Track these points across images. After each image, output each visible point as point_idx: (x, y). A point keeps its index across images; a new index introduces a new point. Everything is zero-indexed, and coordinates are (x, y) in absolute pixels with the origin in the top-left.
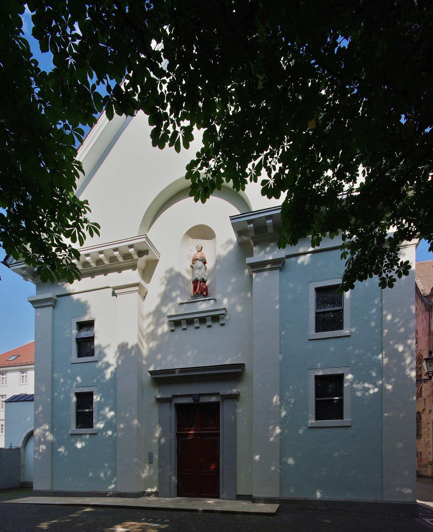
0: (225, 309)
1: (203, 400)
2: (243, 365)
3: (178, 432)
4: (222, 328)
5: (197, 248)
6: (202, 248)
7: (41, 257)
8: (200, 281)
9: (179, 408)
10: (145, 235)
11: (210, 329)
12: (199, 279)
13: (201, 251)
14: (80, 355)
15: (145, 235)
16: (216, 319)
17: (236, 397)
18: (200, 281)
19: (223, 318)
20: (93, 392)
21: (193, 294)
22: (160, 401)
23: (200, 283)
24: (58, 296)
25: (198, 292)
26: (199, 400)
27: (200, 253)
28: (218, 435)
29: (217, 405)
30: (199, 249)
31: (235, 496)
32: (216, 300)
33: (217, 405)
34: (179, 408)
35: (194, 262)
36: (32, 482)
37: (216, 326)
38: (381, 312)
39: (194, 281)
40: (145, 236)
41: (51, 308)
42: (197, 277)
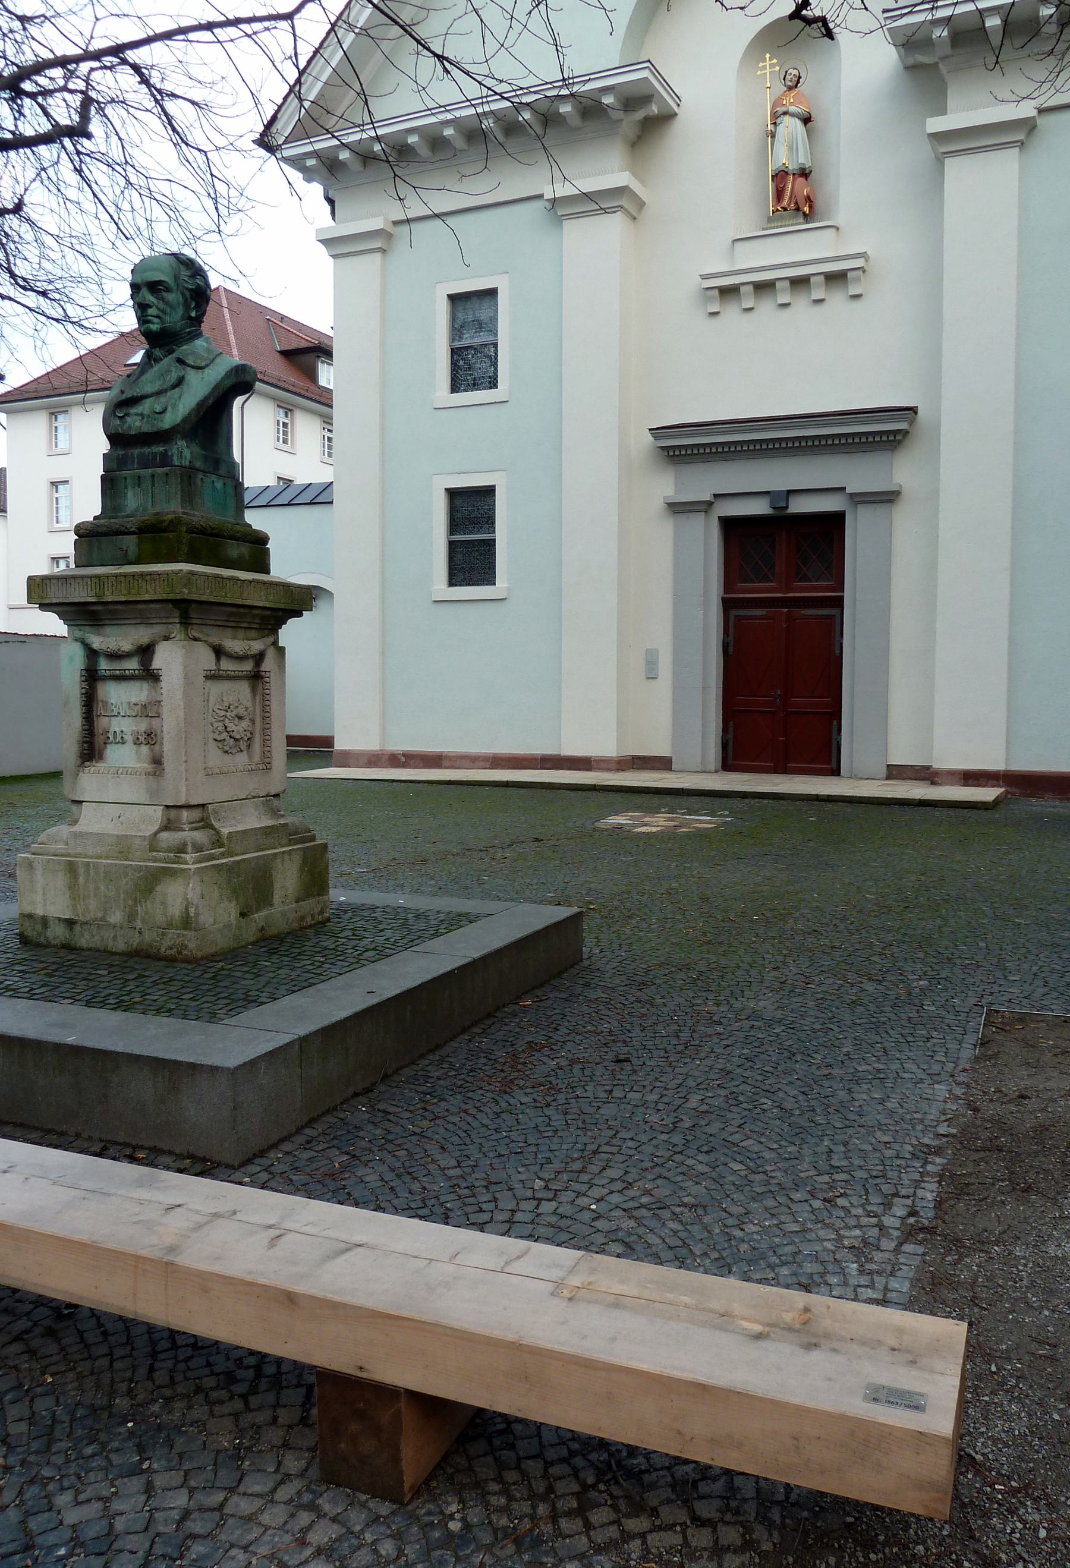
0: (863, 255)
1: (800, 506)
2: (913, 410)
3: (726, 596)
4: (856, 305)
5: (784, 79)
6: (800, 77)
7: (69, 67)
8: (794, 174)
9: (729, 524)
10: (649, 61)
11: (819, 308)
12: (790, 168)
13: (796, 86)
14: (455, 388)
15: (649, 61)
16: (837, 279)
17: (888, 498)
18: (794, 174)
19: (858, 280)
20: (494, 486)
21: (773, 212)
22: (677, 508)
23: (794, 180)
24: (1041, 111)
25: (789, 205)
26: (787, 507)
27: (793, 93)
28: (839, 602)
29: (834, 522)
30: (790, 84)
31: (884, 771)
32: (838, 229)
33: (834, 522)
34: (729, 524)
35: (778, 121)
36: (332, 738)
37: (837, 300)
38: (158, 87)
39: (777, 174)
40: (648, 64)
41: (378, 256)
42: (784, 164)
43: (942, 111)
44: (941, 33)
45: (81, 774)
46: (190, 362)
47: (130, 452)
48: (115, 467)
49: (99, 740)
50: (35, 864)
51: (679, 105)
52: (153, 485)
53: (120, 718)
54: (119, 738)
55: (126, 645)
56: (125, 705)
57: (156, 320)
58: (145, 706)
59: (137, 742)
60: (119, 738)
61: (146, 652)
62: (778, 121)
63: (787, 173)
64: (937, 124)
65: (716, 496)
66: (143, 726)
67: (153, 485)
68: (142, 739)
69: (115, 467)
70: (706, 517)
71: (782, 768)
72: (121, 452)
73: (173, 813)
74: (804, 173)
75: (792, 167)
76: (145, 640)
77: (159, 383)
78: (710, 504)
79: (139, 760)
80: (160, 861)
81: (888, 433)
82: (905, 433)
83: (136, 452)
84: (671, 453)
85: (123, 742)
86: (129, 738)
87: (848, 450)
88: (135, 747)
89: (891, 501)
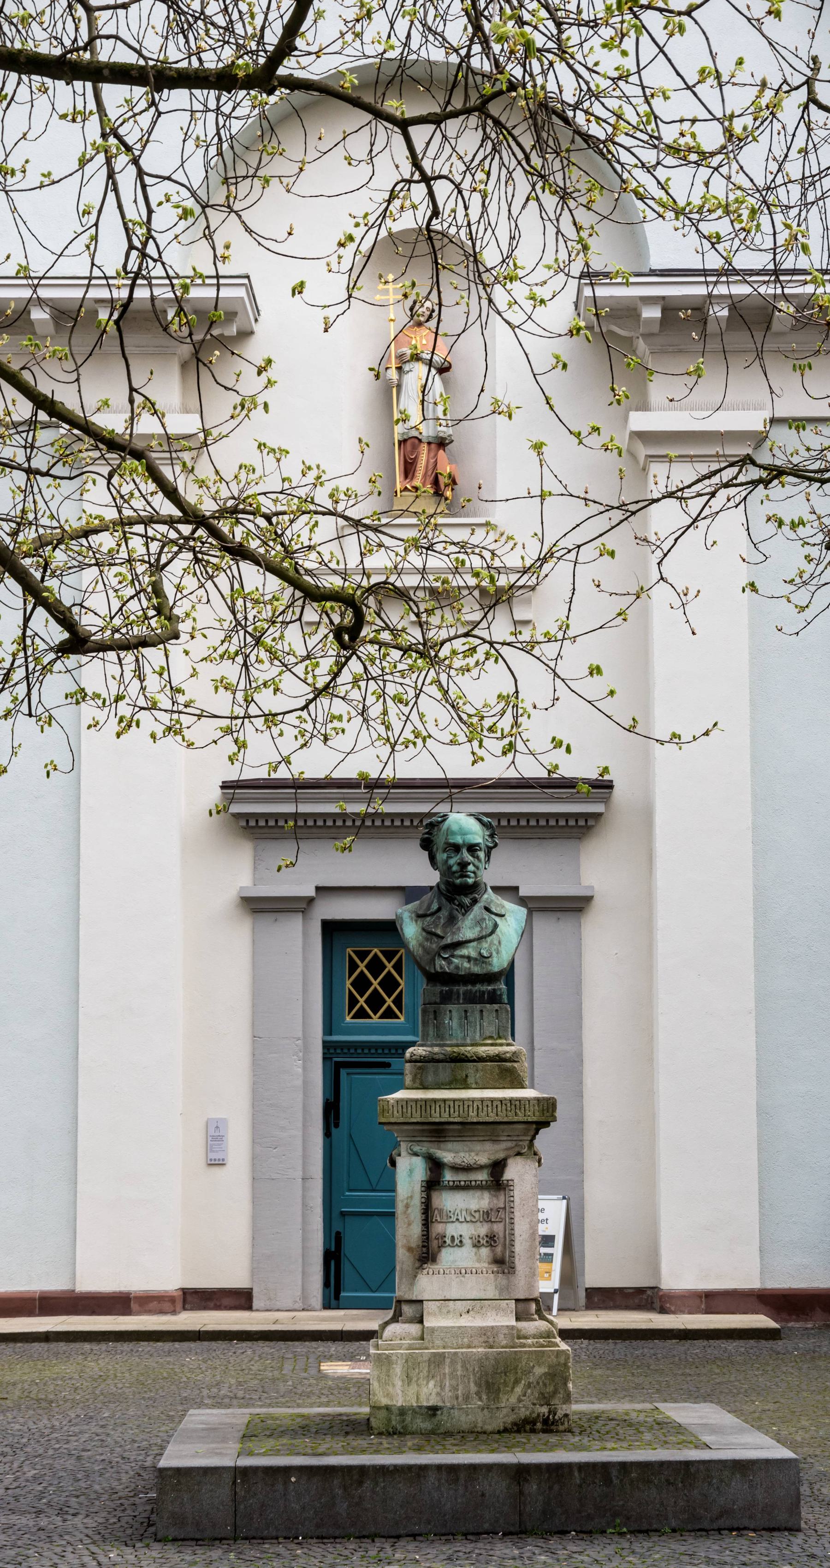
8: (429, 443)
12: (424, 434)
15: (248, 277)
35: (406, 367)
40: (246, 281)
43: (644, 406)
44: (653, 313)
45: (419, 1276)
46: (494, 910)
47: (455, 988)
48: (438, 1000)
49: (434, 1244)
50: (394, 1358)
51: (256, 320)
52: (482, 1018)
53: (457, 1224)
54: (457, 1242)
55: (483, 1159)
56: (464, 1213)
57: (472, 875)
58: (488, 1213)
59: (477, 1245)
60: (457, 1242)
61: (497, 1167)
62: (406, 367)
63: (420, 441)
64: (639, 421)
65: (318, 889)
66: (483, 1230)
67: (482, 1018)
68: (483, 1242)
69: (438, 1000)
70: (304, 919)
71: (356, 1291)
72: (446, 988)
73: (521, 1306)
74: (441, 443)
75: (427, 431)
76: (501, 1156)
77: (478, 929)
78: (310, 901)
79: (479, 1260)
80: (530, 1346)
81: (577, 816)
82: (597, 816)
83: (462, 989)
84: (252, 823)
85: (461, 1244)
86: (467, 1241)
87: (519, 835)
88: (474, 1250)
89: (580, 910)
